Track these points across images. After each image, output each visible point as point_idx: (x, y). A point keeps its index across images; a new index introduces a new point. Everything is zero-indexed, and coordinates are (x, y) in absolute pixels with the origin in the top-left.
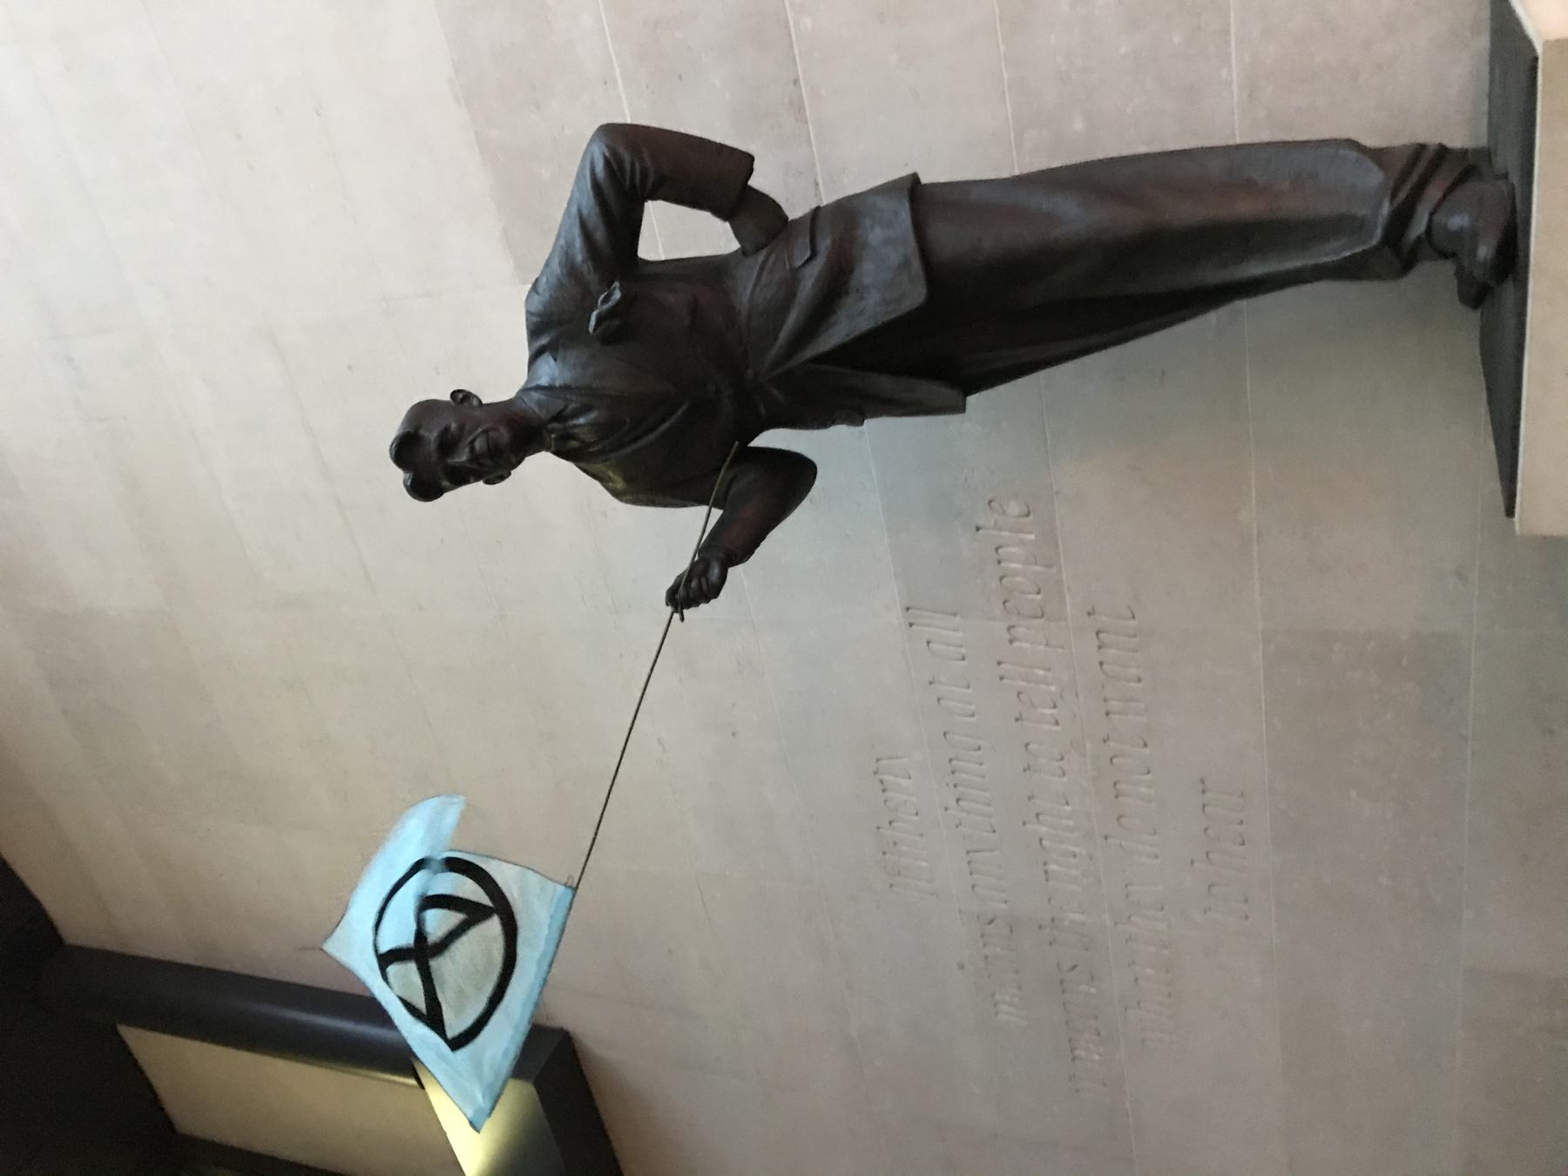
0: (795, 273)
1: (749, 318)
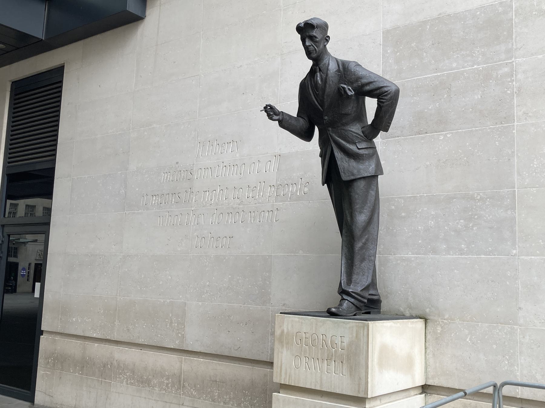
0: (354, 143)
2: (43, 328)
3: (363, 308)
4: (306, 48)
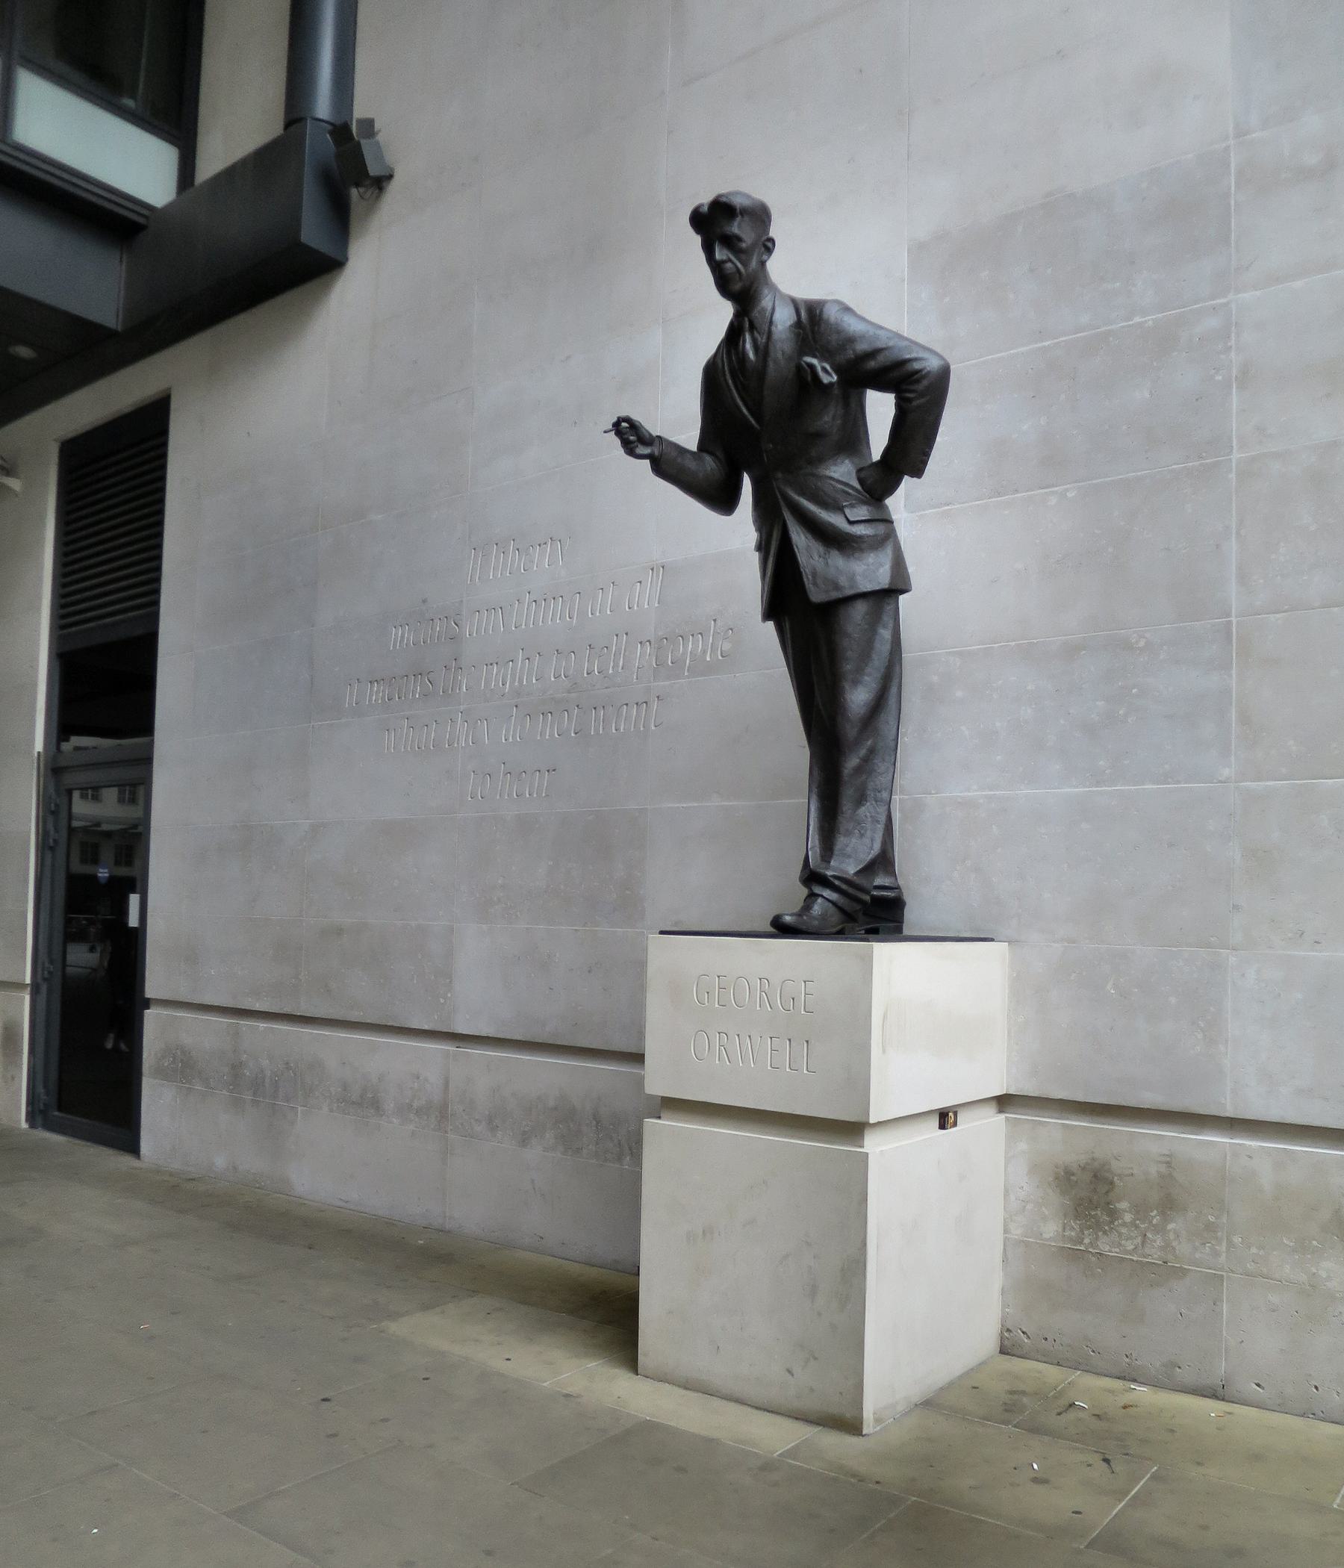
0: (840, 509)
1: (813, 475)
2: (150, 992)
3: (861, 917)
4: (716, 267)
